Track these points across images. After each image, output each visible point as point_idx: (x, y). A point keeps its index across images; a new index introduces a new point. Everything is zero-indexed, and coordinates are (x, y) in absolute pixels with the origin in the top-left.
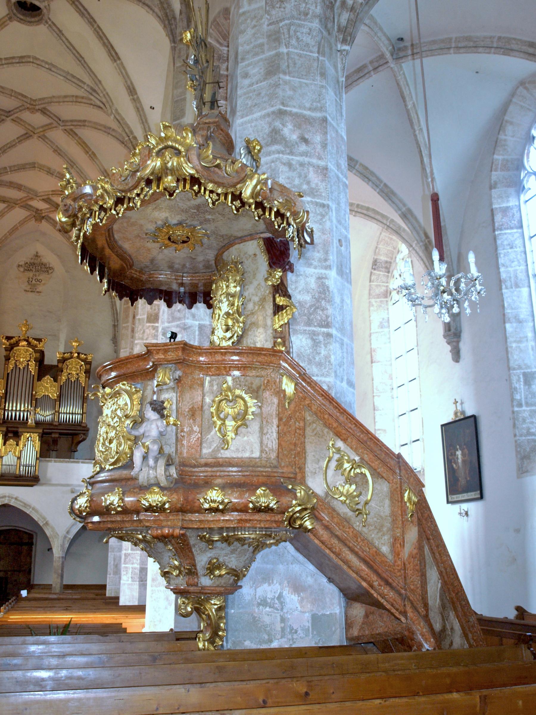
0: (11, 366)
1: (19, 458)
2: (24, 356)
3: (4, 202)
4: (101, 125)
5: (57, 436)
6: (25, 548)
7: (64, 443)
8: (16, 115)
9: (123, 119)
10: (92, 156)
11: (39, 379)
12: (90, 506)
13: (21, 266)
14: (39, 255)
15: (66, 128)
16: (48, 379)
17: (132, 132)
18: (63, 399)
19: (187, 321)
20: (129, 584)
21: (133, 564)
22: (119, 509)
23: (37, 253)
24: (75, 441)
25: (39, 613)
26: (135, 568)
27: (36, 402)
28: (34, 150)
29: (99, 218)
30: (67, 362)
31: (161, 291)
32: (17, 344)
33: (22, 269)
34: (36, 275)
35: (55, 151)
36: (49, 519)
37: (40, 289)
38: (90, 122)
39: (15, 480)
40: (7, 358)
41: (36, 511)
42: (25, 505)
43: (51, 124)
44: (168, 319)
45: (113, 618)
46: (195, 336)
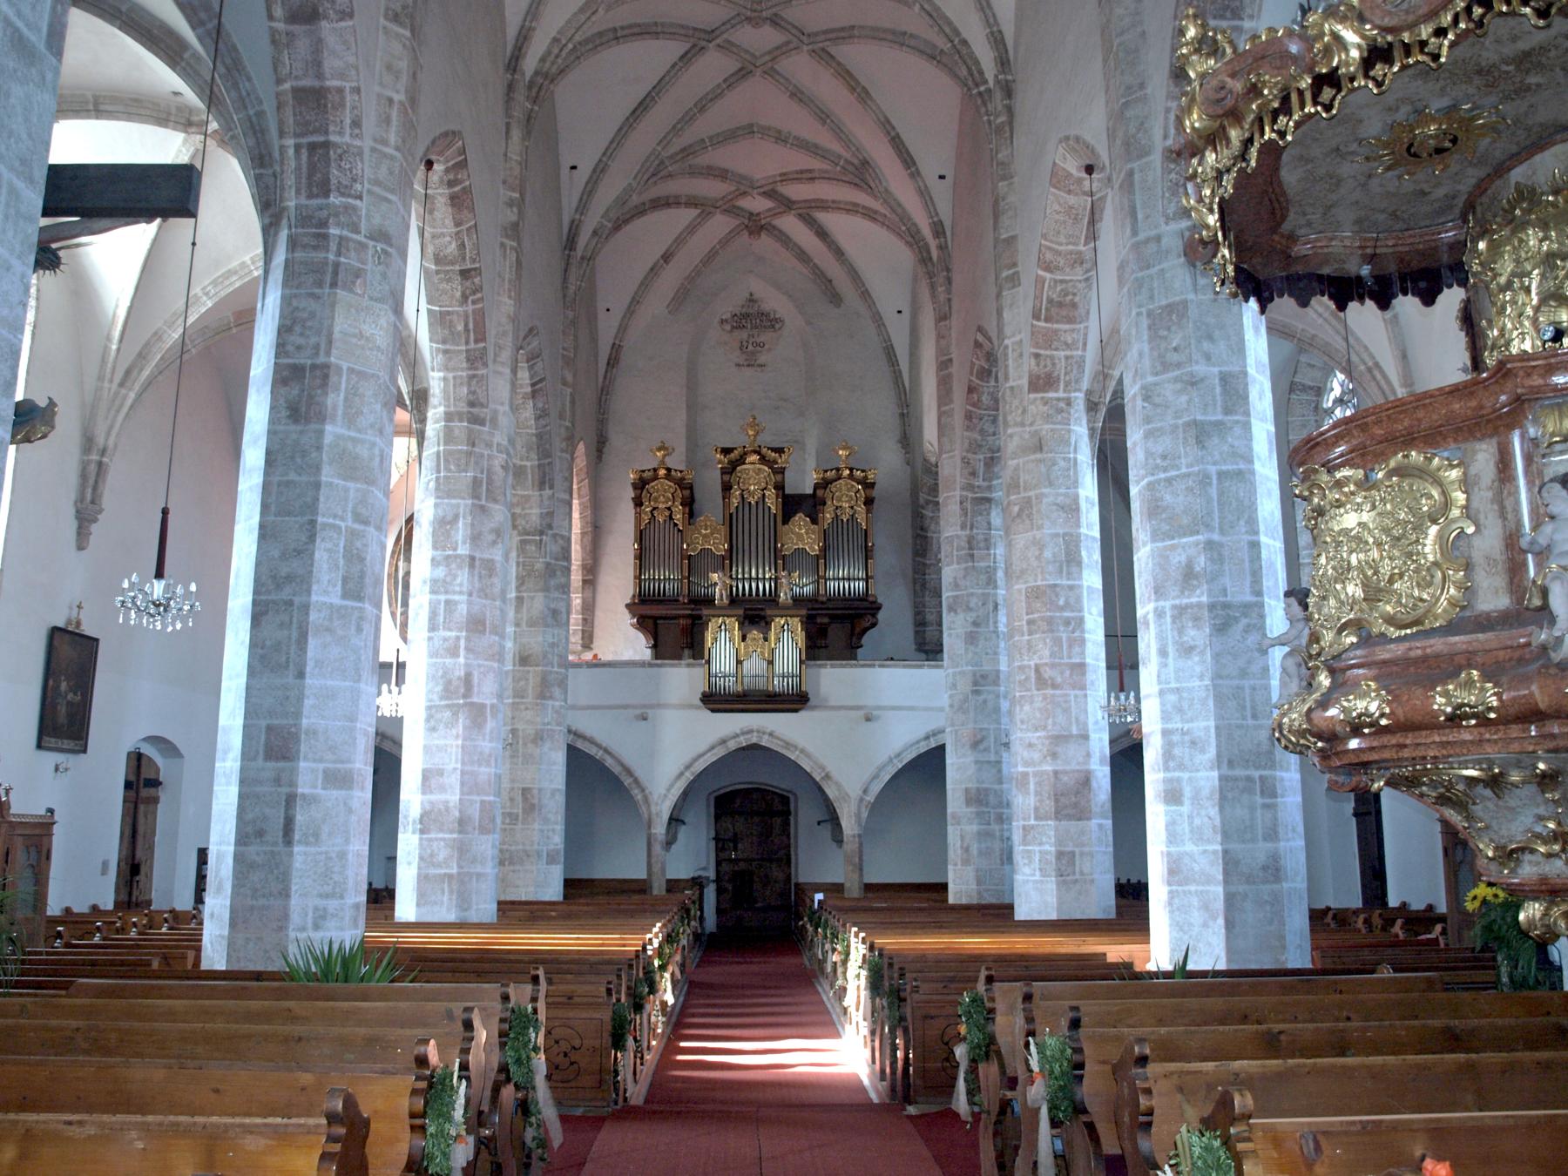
0: (735, 502)
1: (771, 663)
2: (754, 477)
3: (696, 206)
4: (885, 31)
5: (826, 620)
6: (778, 821)
7: (837, 633)
8: (725, 36)
9: (938, 9)
10: (863, 95)
11: (785, 521)
12: (1392, 712)
15: (816, 47)
16: (800, 522)
17: (958, 33)
18: (830, 555)
19: (1196, 368)
20: (1036, 882)
21: (1041, 844)
22: (1384, 722)
24: (858, 630)
25: (926, 934)
26: (1046, 853)
27: (781, 560)
28: (759, 101)
29: (1315, 103)
30: (832, 487)
31: (1320, 278)
32: (741, 460)
33: (728, 327)
35: (793, 95)
36: (831, 768)
37: (762, 359)
38: (862, 27)
39: (766, 702)
40: (727, 488)
41: (808, 756)
42: (788, 745)
43: (788, 43)
44: (1153, 366)
45: (1060, 943)
46: (1214, 397)
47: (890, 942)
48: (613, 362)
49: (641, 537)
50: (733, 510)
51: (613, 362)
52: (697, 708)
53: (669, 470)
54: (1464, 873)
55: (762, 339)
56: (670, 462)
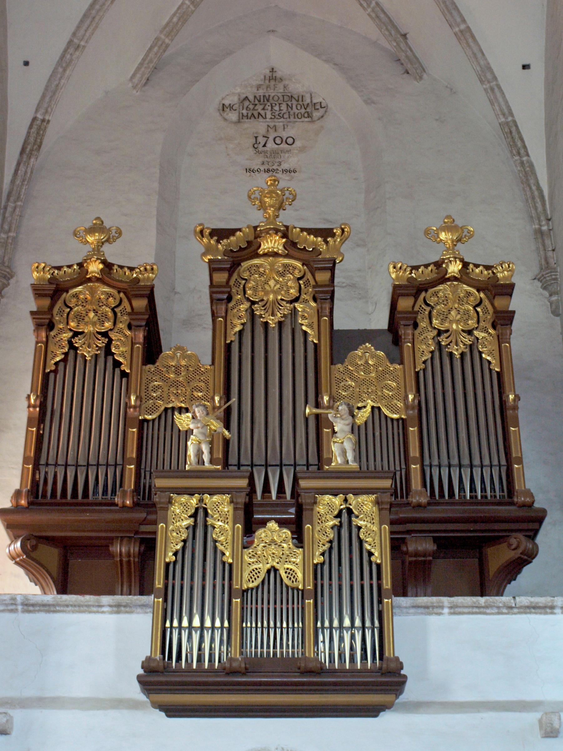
13: (231, 107)
14: (278, 74)
23: (272, 70)
32: (250, 249)
33: (233, 116)
34: (275, 129)
47: (203, 467)
48: (32, 146)
49: (45, 383)
50: (232, 337)
51: (32, 146)
52: (133, 705)
53: (108, 266)
54: (342, 641)
55: (291, 132)
56: (111, 253)
